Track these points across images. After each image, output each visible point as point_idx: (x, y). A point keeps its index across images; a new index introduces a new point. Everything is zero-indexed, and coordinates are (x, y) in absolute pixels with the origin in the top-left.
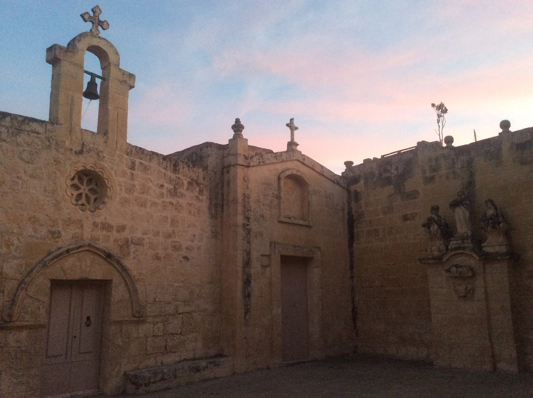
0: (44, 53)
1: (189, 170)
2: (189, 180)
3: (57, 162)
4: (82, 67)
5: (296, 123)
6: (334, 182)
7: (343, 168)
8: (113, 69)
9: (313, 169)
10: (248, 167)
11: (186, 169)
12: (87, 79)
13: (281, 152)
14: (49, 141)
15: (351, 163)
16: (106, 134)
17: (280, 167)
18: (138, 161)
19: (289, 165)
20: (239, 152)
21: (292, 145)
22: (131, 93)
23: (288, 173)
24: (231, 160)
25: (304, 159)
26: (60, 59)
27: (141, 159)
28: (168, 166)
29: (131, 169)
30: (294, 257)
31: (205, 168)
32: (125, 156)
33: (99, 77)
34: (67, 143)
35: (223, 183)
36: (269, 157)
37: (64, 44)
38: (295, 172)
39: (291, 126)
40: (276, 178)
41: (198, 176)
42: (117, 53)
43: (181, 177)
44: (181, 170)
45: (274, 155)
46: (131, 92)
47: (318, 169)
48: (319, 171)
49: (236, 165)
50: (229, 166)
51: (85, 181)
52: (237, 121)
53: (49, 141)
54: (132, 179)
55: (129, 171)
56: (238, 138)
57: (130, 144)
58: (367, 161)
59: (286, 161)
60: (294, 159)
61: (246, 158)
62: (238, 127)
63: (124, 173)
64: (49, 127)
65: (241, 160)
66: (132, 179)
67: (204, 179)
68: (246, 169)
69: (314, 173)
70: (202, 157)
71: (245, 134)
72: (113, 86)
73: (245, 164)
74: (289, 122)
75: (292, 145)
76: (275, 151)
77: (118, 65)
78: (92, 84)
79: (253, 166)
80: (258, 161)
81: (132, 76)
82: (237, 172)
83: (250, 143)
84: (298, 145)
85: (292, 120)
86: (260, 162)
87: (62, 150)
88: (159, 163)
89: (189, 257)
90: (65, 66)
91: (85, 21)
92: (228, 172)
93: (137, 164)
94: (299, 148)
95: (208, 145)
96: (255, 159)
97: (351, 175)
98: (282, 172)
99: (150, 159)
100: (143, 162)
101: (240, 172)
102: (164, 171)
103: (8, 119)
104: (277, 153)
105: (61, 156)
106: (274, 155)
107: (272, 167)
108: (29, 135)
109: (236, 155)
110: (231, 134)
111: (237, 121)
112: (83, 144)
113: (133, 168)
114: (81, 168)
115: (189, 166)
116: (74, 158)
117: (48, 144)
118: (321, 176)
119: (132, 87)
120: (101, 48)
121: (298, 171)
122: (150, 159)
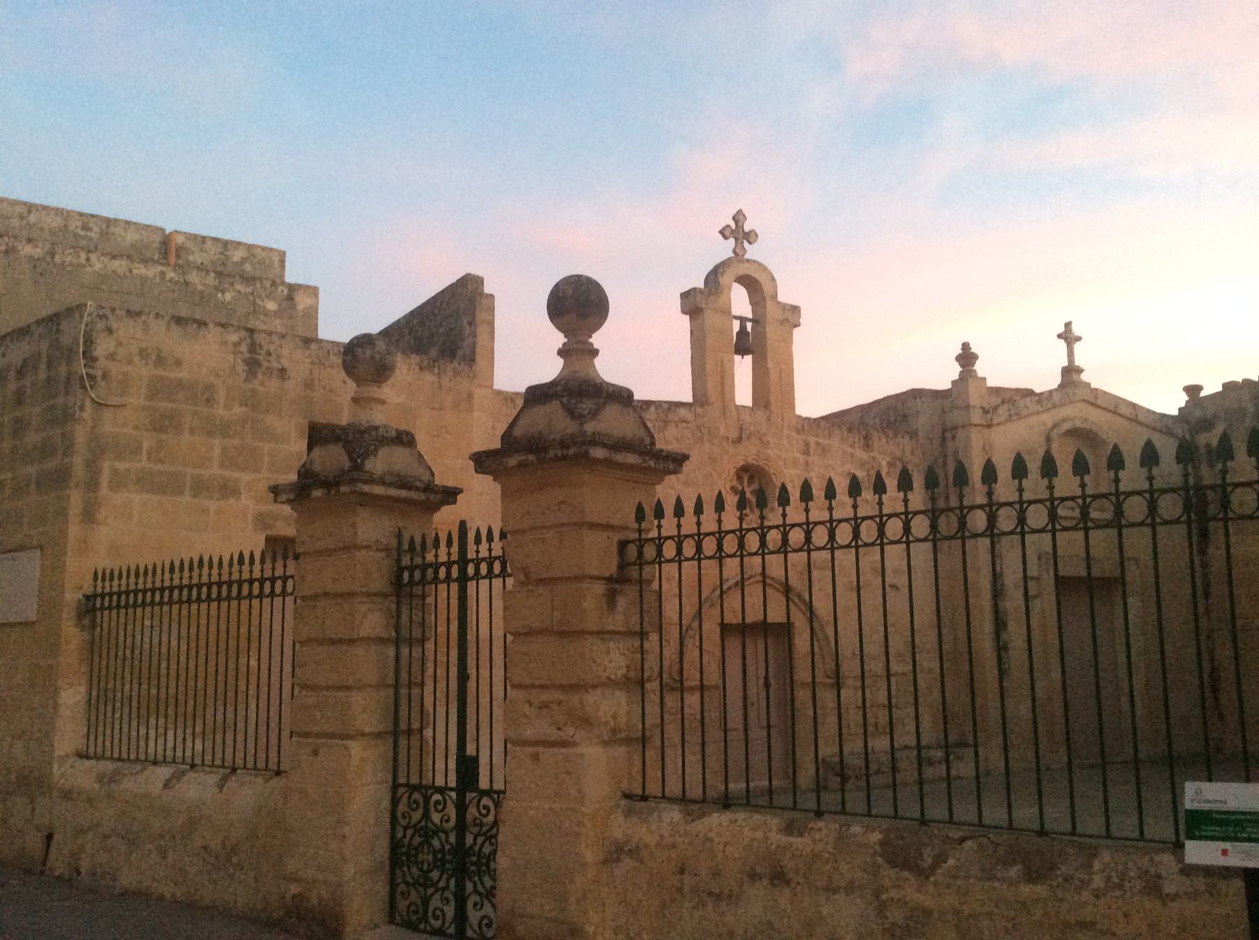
0: (678, 301)
1: (888, 442)
2: (888, 459)
3: (712, 459)
4: (730, 312)
5: (1076, 330)
6: (1160, 431)
7: (1182, 399)
8: (770, 304)
9: (1114, 413)
10: (989, 426)
11: (884, 441)
12: (736, 326)
13: (1051, 392)
14: (701, 431)
15: (1199, 388)
16: (767, 406)
17: (1048, 418)
18: (812, 440)
19: (1067, 411)
20: (973, 403)
21: (1070, 372)
22: (796, 332)
23: (1066, 427)
24: (956, 417)
25: (1096, 397)
26: (702, 309)
27: (817, 436)
28: (856, 440)
29: (804, 453)
30: (134, 893)
31: (913, 435)
32: (796, 436)
33: (749, 320)
34: (722, 431)
35: (945, 456)
36: (1028, 404)
37: (700, 284)
38: (1078, 424)
39: (1068, 337)
40: (1042, 439)
41: (903, 450)
42: (773, 279)
43: (876, 455)
44: (876, 445)
45: (1037, 398)
46: (796, 331)
47: (1124, 410)
48: (1128, 415)
49: (967, 426)
50: (955, 428)
51: (746, 481)
52: (966, 346)
53: (701, 431)
54: (807, 470)
55: (801, 458)
56: (970, 380)
57: (800, 417)
58: (1229, 387)
59: (1062, 405)
60: (1077, 398)
61: (986, 412)
62: (967, 358)
63: (795, 463)
64: (699, 410)
65: (976, 417)
66: (807, 470)
67: (913, 453)
68: (985, 431)
69: (1121, 420)
70: (906, 416)
71: (980, 368)
72: (772, 331)
73: (984, 423)
74: (1062, 329)
75: (1070, 372)
76: (1038, 390)
77: (775, 296)
78: (742, 332)
79: (998, 424)
80: (1007, 413)
81: (795, 310)
82: (968, 437)
83: (990, 383)
84: (1082, 371)
85: (1068, 325)
86: (1010, 416)
87: (716, 441)
88: (842, 439)
89: (898, 585)
90: (710, 318)
91: (726, 238)
92: (954, 437)
93: (812, 445)
94: (1084, 377)
95: (916, 394)
96: (1000, 411)
97: (1198, 413)
98: (1055, 426)
99: (830, 435)
100: (820, 440)
101: (976, 439)
102: (849, 450)
103: (652, 409)
104: (1041, 394)
105: (716, 450)
106: (1037, 398)
107: (1033, 420)
108: (677, 426)
109: (967, 407)
110: (955, 371)
111: (966, 346)
112: (741, 428)
113: (806, 452)
114: (742, 463)
115: (887, 437)
116: (731, 449)
117: (699, 434)
118: (1133, 424)
119: (797, 325)
120: (750, 276)
121: (1086, 420)
122: (830, 435)
